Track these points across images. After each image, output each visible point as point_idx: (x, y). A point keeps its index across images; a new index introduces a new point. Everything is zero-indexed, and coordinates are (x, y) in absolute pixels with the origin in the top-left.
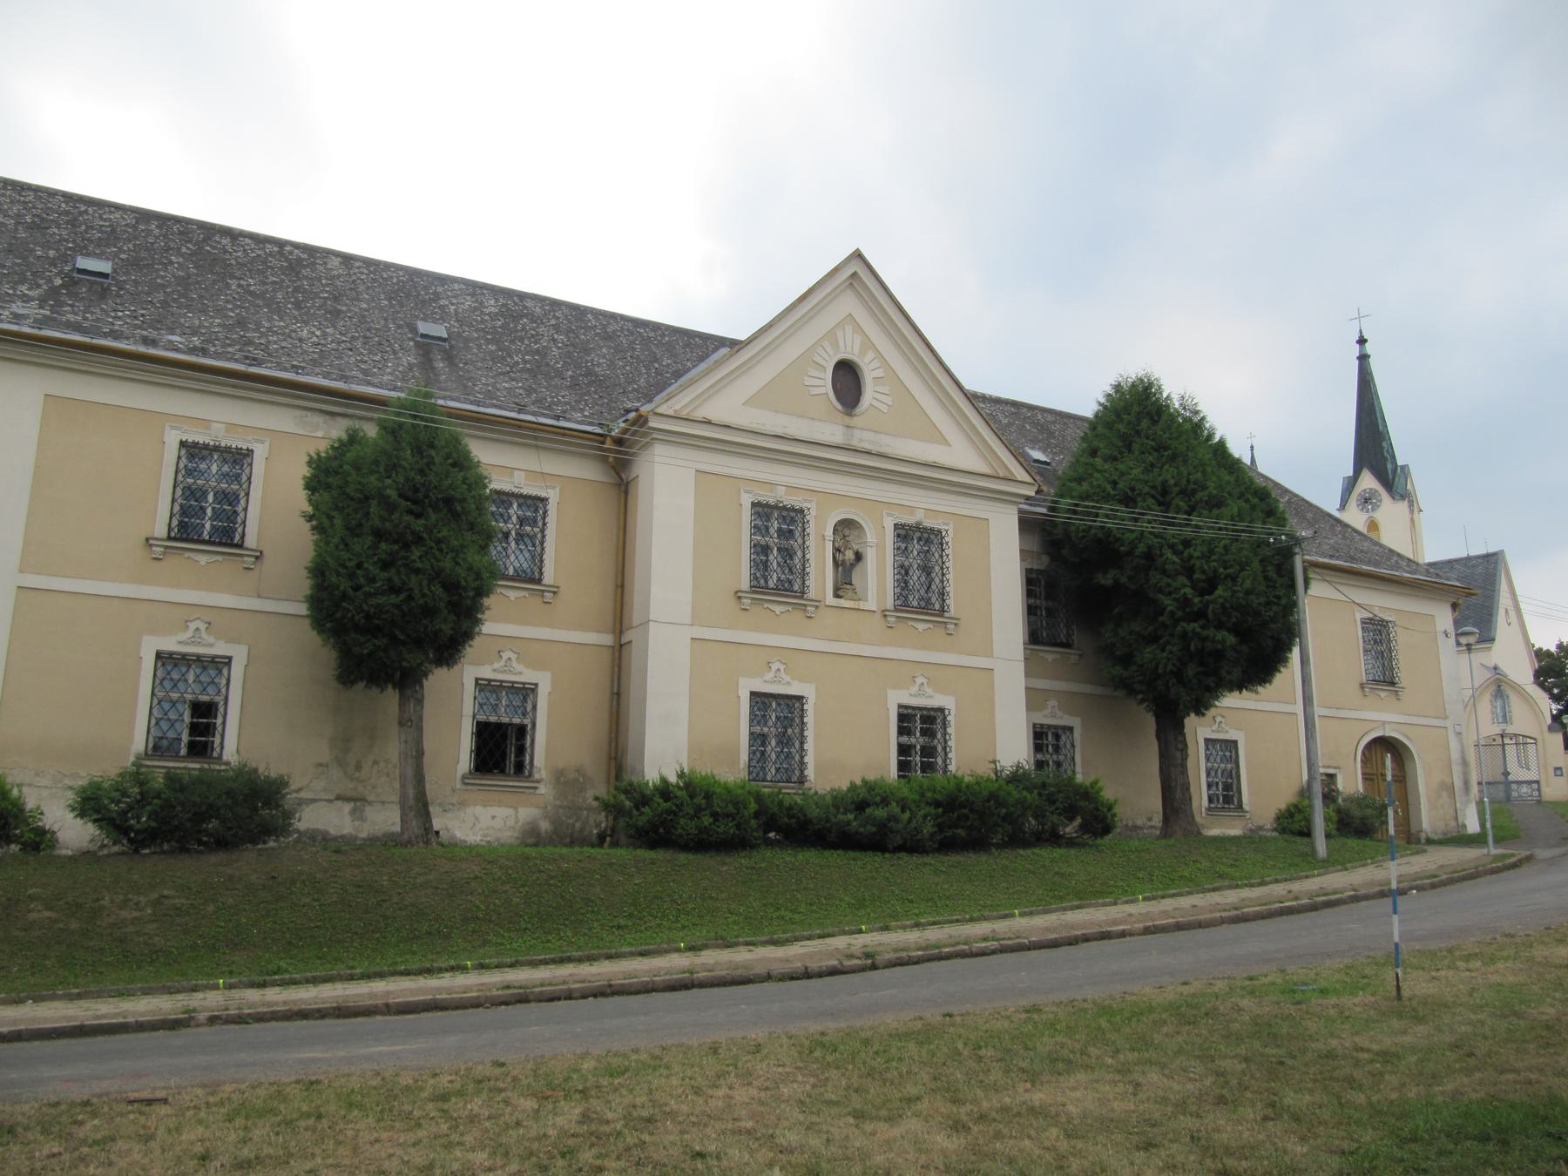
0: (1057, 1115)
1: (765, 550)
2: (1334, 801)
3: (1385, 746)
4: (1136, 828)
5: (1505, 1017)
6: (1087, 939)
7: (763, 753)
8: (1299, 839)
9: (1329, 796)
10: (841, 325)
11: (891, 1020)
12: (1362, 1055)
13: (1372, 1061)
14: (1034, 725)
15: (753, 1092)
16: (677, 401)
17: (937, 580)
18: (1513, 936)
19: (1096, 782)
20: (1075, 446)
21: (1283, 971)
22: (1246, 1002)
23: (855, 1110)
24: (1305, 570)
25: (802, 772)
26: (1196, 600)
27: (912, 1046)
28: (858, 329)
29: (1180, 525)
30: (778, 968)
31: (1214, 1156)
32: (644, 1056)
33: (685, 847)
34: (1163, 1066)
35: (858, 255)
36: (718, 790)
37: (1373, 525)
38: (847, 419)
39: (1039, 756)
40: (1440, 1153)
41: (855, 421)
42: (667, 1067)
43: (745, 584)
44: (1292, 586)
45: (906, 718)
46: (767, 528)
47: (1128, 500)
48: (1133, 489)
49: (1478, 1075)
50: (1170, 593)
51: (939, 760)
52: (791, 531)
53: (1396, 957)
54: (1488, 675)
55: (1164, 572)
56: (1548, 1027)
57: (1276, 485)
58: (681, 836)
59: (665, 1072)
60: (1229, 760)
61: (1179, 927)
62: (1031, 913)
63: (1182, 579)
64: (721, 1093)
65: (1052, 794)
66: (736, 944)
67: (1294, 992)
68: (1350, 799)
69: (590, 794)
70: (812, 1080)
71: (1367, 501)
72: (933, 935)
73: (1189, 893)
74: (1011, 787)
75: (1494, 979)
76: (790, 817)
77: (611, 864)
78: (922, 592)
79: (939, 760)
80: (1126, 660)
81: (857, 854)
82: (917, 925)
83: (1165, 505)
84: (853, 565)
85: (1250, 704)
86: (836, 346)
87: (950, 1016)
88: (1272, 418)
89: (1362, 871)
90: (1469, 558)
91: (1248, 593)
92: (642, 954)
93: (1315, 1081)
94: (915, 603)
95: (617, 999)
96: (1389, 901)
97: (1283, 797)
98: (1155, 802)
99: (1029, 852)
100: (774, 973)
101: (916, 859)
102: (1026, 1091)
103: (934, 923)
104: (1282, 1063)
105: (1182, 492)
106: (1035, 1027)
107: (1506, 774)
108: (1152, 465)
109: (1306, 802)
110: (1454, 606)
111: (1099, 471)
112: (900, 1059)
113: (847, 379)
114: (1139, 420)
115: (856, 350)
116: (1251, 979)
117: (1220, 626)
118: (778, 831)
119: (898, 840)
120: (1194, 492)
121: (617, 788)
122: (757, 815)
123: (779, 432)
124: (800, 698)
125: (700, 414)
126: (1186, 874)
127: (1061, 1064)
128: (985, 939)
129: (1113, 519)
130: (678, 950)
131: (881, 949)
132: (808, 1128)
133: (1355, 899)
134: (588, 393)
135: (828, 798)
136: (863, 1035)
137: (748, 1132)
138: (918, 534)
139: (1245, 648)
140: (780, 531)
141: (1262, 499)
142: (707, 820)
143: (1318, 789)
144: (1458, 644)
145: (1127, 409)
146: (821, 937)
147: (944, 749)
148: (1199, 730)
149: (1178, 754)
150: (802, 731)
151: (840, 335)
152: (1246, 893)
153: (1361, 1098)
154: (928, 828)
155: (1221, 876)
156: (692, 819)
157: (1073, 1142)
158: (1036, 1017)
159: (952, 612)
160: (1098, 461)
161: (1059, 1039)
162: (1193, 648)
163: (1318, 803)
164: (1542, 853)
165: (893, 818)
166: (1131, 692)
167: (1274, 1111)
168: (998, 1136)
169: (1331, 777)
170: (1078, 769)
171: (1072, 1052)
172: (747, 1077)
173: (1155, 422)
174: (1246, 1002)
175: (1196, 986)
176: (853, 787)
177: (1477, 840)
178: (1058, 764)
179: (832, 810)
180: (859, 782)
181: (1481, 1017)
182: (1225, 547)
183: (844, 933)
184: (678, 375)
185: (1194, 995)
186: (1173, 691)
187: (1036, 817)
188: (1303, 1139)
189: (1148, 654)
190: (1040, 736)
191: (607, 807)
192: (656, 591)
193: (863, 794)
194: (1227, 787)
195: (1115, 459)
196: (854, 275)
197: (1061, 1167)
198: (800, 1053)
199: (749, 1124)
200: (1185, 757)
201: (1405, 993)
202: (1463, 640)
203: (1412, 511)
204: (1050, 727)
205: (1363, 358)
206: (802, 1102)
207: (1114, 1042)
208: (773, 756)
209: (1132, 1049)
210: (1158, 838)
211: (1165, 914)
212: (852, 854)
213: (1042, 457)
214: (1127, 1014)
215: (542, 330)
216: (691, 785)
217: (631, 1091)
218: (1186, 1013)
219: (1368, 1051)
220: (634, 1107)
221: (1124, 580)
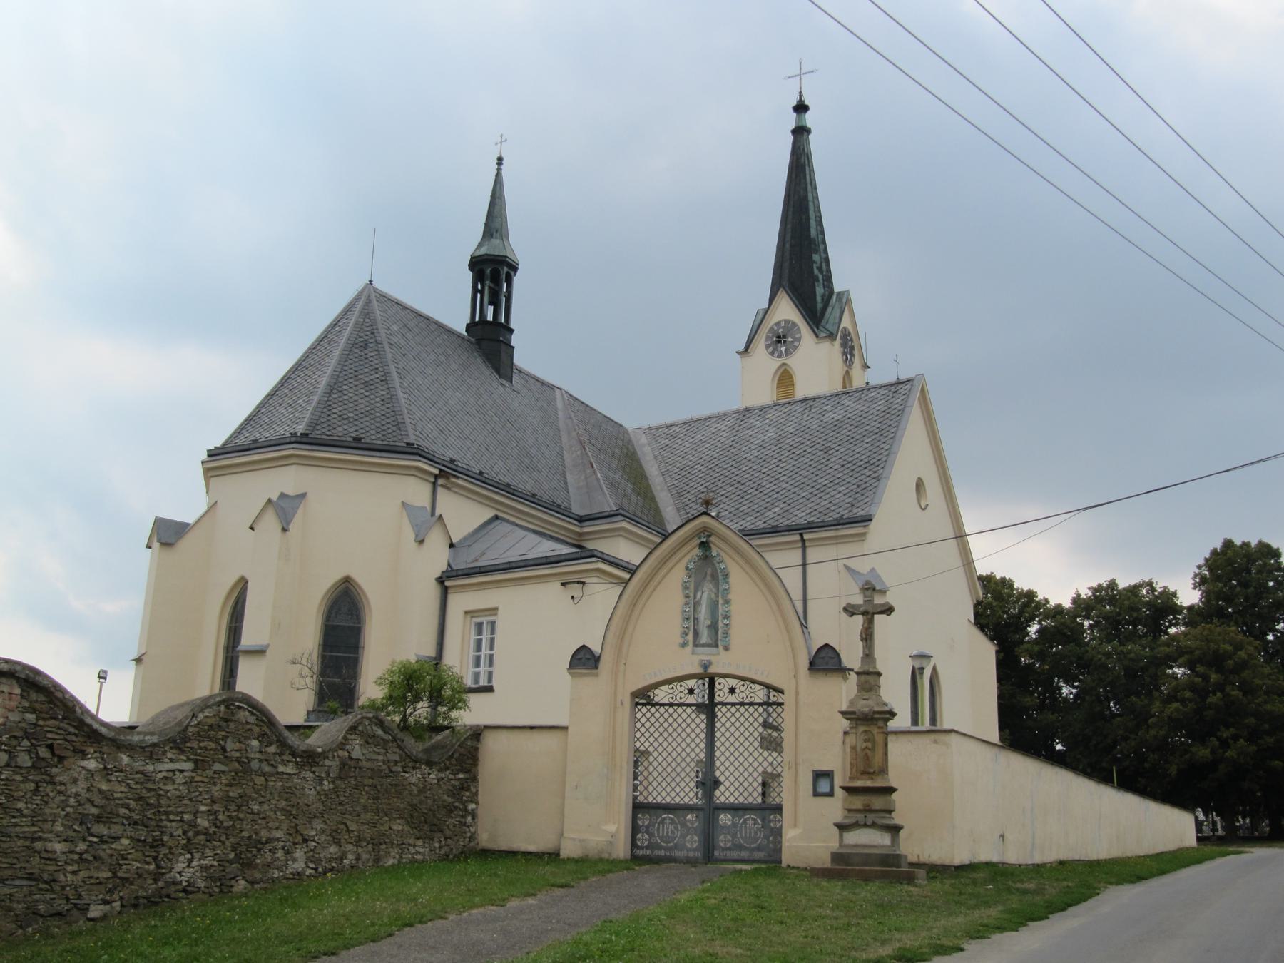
180: (1254, 543)
205: (800, 132)
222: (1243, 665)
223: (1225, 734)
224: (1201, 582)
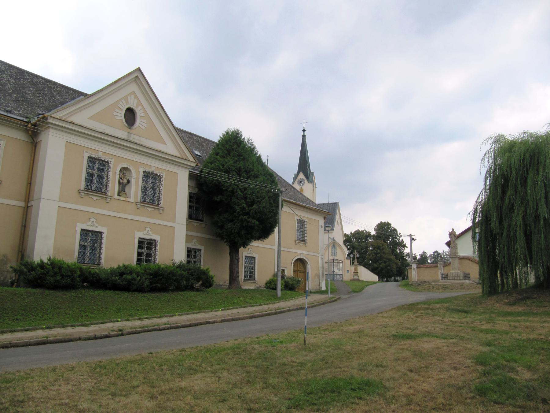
0: (190, 390)
1: (92, 175)
2: (284, 278)
3: (301, 262)
4: (220, 285)
5: (336, 349)
6: (201, 324)
7: (84, 253)
8: (272, 291)
9: (283, 277)
10: (130, 94)
11: (128, 356)
12: (295, 364)
13: (297, 366)
14: (188, 248)
15: (70, 387)
16: (61, 113)
17: (157, 193)
18: (337, 323)
19: (207, 269)
20: (211, 151)
21: (268, 335)
22: (256, 346)
23: (112, 393)
24: (282, 201)
25: (99, 260)
26: (247, 208)
27: (136, 366)
28: (136, 97)
29: (244, 182)
30: (84, 335)
31: (247, 403)
32: (22, 374)
33: (49, 288)
34: (228, 370)
35: (139, 70)
36: (64, 266)
37: (302, 190)
38: (129, 130)
39: (189, 259)
40: (320, 398)
41: (132, 131)
42: (33, 378)
43: (83, 187)
44: (278, 207)
45: (141, 243)
46: (93, 167)
47: (227, 172)
48: (229, 168)
49: (329, 370)
50: (238, 205)
51: (153, 259)
52: (103, 169)
53: (305, 330)
54: (330, 241)
55: (237, 198)
56: (349, 353)
57: (275, 173)
58: (47, 283)
59: (31, 380)
60: (252, 264)
61: (233, 320)
62: (182, 315)
63: (243, 201)
64: (55, 388)
65: (193, 272)
66: (67, 326)
67: (272, 342)
68: (288, 278)
69: (8, 266)
70: (95, 381)
71: (300, 182)
72: (146, 322)
73: (237, 308)
74: (178, 269)
75: (332, 337)
76: (93, 277)
77: (15, 294)
78: (152, 197)
79: (153, 259)
80: (222, 227)
81: (119, 292)
82: (140, 319)
83: (239, 175)
84: (126, 185)
85: (263, 246)
86: (127, 102)
87: (151, 353)
88: (274, 150)
89: (291, 301)
90: (329, 204)
91: (264, 207)
92: (26, 330)
93: (279, 374)
94: (148, 201)
95: (13, 349)
96: (304, 311)
97: (268, 277)
98: (227, 277)
99: (183, 293)
100: (82, 337)
101: (141, 294)
102: (179, 381)
103: (146, 318)
104: (268, 368)
105: (245, 171)
106: (183, 357)
107: (334, 272)
108: (236, 161)
109: (275, 278)
110: (325, 218)
111: (219, 161)
112: (131, 371)
113: (130, 115)
114: (234, 145)
115: (135, 105)
116: (258, 338)
117: (253, 218)
118: (88, 282)
119: (135, 287)
120: (249, 172)
121: (21, 264)
122: (79, 276)
123: (102, 131)
124: (101, 233)
125: (70, 119)
126: (236, 302)
127: (192, 371)
128: (165, 324)
129: (221, 177)
130: (42, 329)
131: (124, 328)
132: (92, 401)
133: (289, 311)
134: (22, 105)
135: (109, 271)
136: (117, 362)
137: (66, 404)
138: (152, 176)
139: (261, 226)
140: (98, 169)
141: (271, 177)
142: (59, 278)
143: (280, 274)
144: (325, 230)
145: (230, 140)
146: (102, 323)
147: (155, 254)
148: (243, 252)
149: (236, 261)
150: (101, 245)
151: (129, 98)
152: (255, 308)
153: (294, 379)
154: (146, 283)
155: (247, 302)
156: (52, 277)
157: (196, 401)
158: (183, 353)
159: (162, 206)
160: (218, 157)
161: (192, 361)
162: (244, 225)
163: (279, 279)
164: (343, 297)
165: (134, 279)
166: (222, 238)
167: (266, 385)
168: (168, 400)
169: (283, 270)
170: (202, 264)
171: (196, 366)
172: (67, 381)
173: (239, 146)
174: (256, 346)
175: (240, 341)
176: (119, 267)
177: (325, 292)
178: (195, 262)
179: (110, 275)
180: (121, 265)
181: (329, 349)
182: (258, 192)
183: (111, 322)
184: (62, 103)
185: (239, 344)
186: (236, 239)
187: (186, 281)
188: (276, 395)
189: (229, 226)
190: (190, 252)
191: (15, 271)
192: (45, 187)
193: (123, 269)
194: (251, 272)
195: (224, 157)
196: (137, 77)
197: (192, 411)
198: (91, 370)
199: (67, 401)
200: (238, 261)
201: (307, 342)
202: (327, 229)
203: (313, 187)
204: (193, 249)
205: (304, 136)
206: (90, 390)
207: (211, 362)
208: (88, 254)
209: (218, 364)
210: (227, 289)
211: (229, 315)
212: (117, 292)
213: (199, 154)
214: (216, 351)
215: (4, 76)
216: (53, 264)
217: (15, 389)
218: (237, 351)
219: (296, 362)
220: (15, 396)
221: (223, 199)
222: (383, 249)
223: (380, 262)
224: (375, 230)
